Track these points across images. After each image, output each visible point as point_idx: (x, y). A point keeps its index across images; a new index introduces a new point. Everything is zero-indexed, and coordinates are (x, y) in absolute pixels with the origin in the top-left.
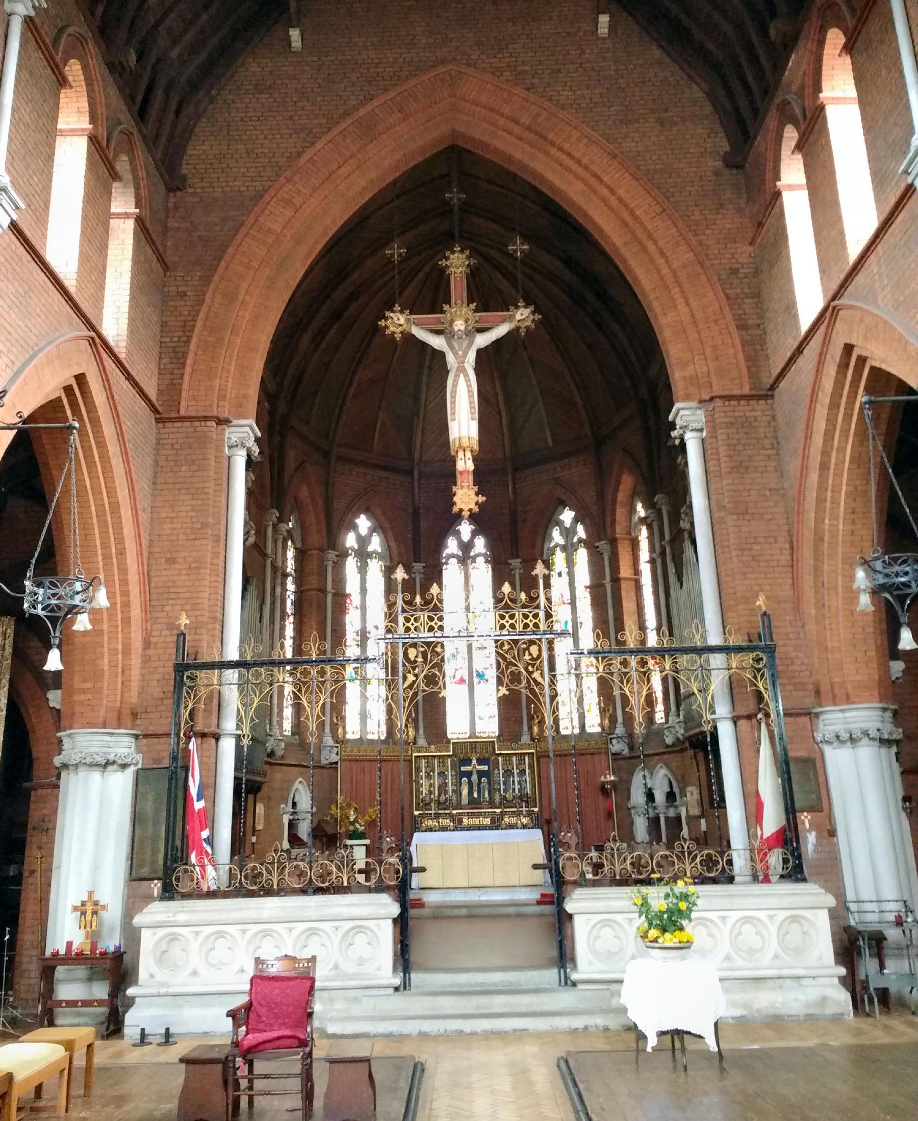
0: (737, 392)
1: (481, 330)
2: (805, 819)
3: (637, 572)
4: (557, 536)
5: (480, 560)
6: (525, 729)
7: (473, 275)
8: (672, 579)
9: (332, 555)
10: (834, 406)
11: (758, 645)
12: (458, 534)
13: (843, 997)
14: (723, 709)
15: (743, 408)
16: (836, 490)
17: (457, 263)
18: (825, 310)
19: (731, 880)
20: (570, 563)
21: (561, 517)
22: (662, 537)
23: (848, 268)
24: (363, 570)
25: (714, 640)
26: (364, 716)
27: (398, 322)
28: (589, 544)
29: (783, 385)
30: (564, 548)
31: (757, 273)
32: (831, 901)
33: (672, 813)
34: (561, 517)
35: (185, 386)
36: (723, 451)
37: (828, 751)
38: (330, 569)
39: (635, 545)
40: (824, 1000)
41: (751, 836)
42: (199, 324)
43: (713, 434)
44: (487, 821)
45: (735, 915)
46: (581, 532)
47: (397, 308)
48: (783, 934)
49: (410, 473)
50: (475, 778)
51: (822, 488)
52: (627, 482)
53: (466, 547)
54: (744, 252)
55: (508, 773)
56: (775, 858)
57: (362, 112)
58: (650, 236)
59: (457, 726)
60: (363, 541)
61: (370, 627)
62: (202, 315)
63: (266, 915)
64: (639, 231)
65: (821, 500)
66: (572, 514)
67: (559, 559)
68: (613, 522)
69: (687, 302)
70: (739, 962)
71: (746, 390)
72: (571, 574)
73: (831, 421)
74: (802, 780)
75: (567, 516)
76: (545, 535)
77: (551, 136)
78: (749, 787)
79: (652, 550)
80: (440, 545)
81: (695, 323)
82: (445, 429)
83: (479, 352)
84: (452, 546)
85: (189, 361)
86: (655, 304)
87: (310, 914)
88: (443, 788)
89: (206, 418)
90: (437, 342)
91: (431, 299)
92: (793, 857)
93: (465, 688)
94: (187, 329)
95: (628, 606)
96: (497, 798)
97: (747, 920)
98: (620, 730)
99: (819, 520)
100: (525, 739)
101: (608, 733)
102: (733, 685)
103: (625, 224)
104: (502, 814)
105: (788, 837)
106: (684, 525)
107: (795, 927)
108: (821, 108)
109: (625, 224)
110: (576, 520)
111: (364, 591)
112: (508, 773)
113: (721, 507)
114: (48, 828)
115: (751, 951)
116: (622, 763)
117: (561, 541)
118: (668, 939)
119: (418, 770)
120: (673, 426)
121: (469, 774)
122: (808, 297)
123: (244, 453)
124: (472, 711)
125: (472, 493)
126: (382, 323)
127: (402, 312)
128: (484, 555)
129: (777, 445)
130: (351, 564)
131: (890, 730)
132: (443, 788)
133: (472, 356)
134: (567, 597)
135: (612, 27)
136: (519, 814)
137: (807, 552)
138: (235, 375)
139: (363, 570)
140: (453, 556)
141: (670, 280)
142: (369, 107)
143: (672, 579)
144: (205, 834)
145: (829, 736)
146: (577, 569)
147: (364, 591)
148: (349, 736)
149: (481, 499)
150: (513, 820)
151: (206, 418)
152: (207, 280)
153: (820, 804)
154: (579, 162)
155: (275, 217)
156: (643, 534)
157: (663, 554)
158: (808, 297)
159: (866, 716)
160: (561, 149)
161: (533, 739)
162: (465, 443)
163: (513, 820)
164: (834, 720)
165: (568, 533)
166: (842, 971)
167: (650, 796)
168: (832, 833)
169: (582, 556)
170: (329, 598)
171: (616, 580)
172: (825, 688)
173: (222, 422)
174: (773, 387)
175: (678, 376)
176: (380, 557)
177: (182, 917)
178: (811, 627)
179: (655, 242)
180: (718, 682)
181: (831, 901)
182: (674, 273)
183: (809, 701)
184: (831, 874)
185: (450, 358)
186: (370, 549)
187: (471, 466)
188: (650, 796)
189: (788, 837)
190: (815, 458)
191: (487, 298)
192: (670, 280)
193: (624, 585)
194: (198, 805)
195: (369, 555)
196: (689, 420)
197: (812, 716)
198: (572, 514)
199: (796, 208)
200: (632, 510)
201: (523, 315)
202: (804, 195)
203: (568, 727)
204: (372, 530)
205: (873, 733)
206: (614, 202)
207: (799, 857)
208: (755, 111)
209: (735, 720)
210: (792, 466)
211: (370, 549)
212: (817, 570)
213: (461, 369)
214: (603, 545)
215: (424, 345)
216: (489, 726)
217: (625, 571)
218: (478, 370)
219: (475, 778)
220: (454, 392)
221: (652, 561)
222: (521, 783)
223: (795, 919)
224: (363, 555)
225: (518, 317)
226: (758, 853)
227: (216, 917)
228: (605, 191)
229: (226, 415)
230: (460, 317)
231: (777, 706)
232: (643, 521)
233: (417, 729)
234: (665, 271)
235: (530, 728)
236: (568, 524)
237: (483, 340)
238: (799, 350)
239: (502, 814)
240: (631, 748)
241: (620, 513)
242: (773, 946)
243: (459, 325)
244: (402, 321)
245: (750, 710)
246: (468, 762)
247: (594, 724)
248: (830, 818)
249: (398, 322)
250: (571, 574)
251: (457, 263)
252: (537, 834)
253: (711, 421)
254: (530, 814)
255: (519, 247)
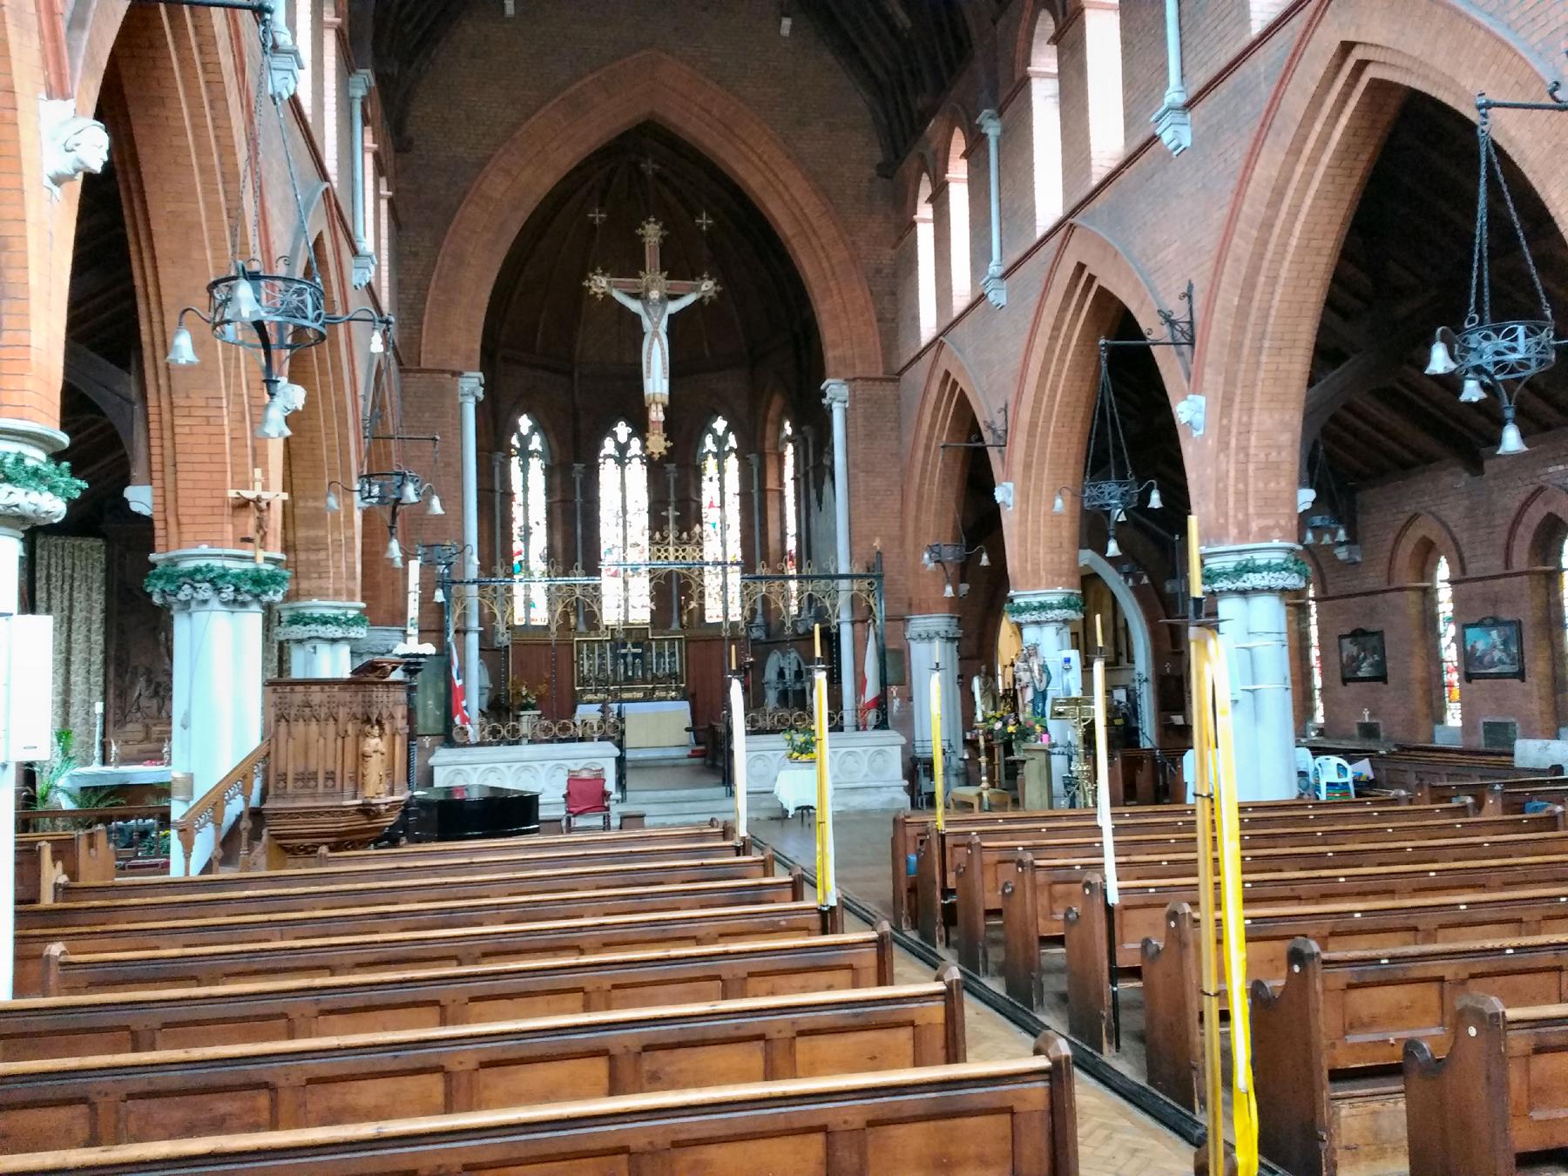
0: (873, 375)
1: (674, 298)
2: (894, 690)
3: (782, 484)
4: (709, 444)
5: (637, 461)
6: (675, 615)
7: (665, 246)
8: (814, 503)
9: (499, 455)
10: (937, 408)
11: (873, 572)
12: (614, 435)
13: (906, 799)
14: (845, 615)
15: (877, 389)
16: (934, 465)
17: (652, 233)
18: (936, 339)
19: (842, 730)
20: (721, 470)
21: (715, 425)
22: (806, 464)
23: (950, 321)
24: (525, 469)
25: (844, 568)
26: (528, 604)
27: (600, 284)
28: (741, 454)
29: (907, 374)
30: (716, 455)
31: (895, 275)
32: (903, 740)
33: (798, 686)
34: (715, 425)
35: (424, 341)
36: (860, 421)
37: (913, 644)
38: (497, 470)
39: (781, 459)
40: (893, 799)
41: (857, 701)
42: (433, 284)
43: (853, 407)
44: (640, 695)
45: (844, 750)
46: (732, 441)
47: (599, 271)
48: (871, 761)
49: (570, 374)
50: (630, 659)
51: (925, 463)
52: (777, 403)
53: (622, 448)
54: (888, 254)
55: (660, 655)
56: (872, 716)
57: (573, 89)
58: (814, 231)
59: (610, 615)
60: (525, 440)
61: (532, 523)
62: (435, 277)
63: (526, 756)
64: (806, 226)
65: (924, 471)
66: (725, 423)
67: (711, 465)
68: (763, 438)
69: (840, 292)
70: (842, 779)
71: (880, 374)
72: (721, 480)
73: (934, 417)
74: (894, 667)
75: (720, 425)
76: (700, 442)
77: (737, 131)
78: (860, 663)
79: (796, 466)
80: (598, 447)
81: (845, 312)
82: (641, 388)
83: (670, 316)
84: (609, 446)
85: (426, 319)
86: (816, 291)
87: (557, 755)
88: (602, 667)
89: (443, 371)
90: (635, 306)
91: (629, 264)
92: (881, 715)
93: (619, 581)
94: (422, 290)
95: (772, 515)
96: (649, 676)
97: (849, 753)
98: (759, 620)
99: (921, 485)
100: (675, 626)
101: (750, 623)
102: (854, 601)
103: (796, 219)
104: (654, 689)
105: (881, 703)
106: (826, 462)
107: (879, 759)
108: (946, 184)
109: (796, 219)
110: (728, 430)
111: (526, 489)
112: (660, 655)
113: (855, 465)
114: (1291, 659)
115: (851, 772)
116: (760, 648)
117: (714, 449)
118: (804, 758)
119: (579, 652)
120: (824, 395)
121: (624, 656)
122: (928, 326)
123: (472, 400)
124: (624, 599)
125: (662, 439)
126: (586, 284)
127: (603, 275)
128: (641, 457)
129: (898, 420)
130: (515, 462)
131: (954, 631)
132: (602, 667)
133: (664, 322)
134: (717, 502)
135: (793, 28)
136: (667, 689)
137: (912, 505)
138: (462, 326)
139: (525, 469)
140: (610, 456)
141: (829, 274)
142: (578, 85)
143: (814, 503)
144: (464, 703)
145: (914, 635)
146: (727, 476)
147: (526, 489)
148: (517, 623)
149: (669, 444)
150: (663, 694)
151: (443, 371)
152: (438, 244)
153: (904, 680)
154: (760, 158)
155: (495, 185)
156: (790, 450)
157: (806, 474)
158: (928, 326)
159: (938, 622)
160: (744, 142)
161: (682, 626)
162: (658, 398)
163: (663, 694)
164: (920, 624)
165: (720, 441)
166: (906, 783)
167: (781, 674)
168: (911, 699)
169: (732, 463)
170: (498, 499)
171: (763, 490)
172: (915, 602)
173: (457, 374)
174: (900, 374)
175: (830, 355)
176: (541, 455)
177: (465, 759)
178: (910, 558)
179: (818, 237)
180: (843, 601)
181: (903, 740)
182: (832, 267)
183: (904, 610)
184: (906, 724)
185: (647, 324)
186: (531, 448)
187: (661, 417)
188: (781, 674)
189: (881, 703)
190: (923, 441)
191: (678, 267)
192: (829, 274)
193: (770, 495)
194: (458, 683)
195: (531, 454)
196: (836, 392)
197: (905, 621)
198: (725, 423)
199: (925, 234)
200: (781, 428)
201: (707, 286)
202: (931, 226)
203: (713, 614)
204: (533, 430)
205: (943, 634)
206: (787, 197)
207: (886, 714)
208: (905, 141)
209: (853, 623)
210: (908, 439)
211: (531, 448)
212: (917, 519)
213: (656, 334)
214: (753, 457)
215: (622, 307)
216: (641, 613)
217: (771, 484)
218: (670, 334)
219: (630, 659)
220: (650, 353)
221: (795, 479)
222: (671, 662)
223: (879, 753)
224: (525, 454)
225: (703, 288)
226: (860, 711)
227: (486, 758)
228: (780, 187)
229: (457, 368)
230: (655, 283)
231: (880, 611)
232: (789, 439)
233: (577, 616)
234: (825, 265)
235: (680, 617)
236: (720, 433)
237: (674, 307)
238: (918, 357)
239: (654, 689)
240: (768, 635)
241: (770, 430)
242: (865, 769)
243: (655, 294)
244: (604, 284)
245: (863, 616)
246: (624, 646)
247: (736, 614)
248: (910, 689)
249: (600, 284)
250: (721, 480)
251: (652, 233)
252: (686, 705)
253: (853, 395)
254: (677, 689)
255: (704, 221)
